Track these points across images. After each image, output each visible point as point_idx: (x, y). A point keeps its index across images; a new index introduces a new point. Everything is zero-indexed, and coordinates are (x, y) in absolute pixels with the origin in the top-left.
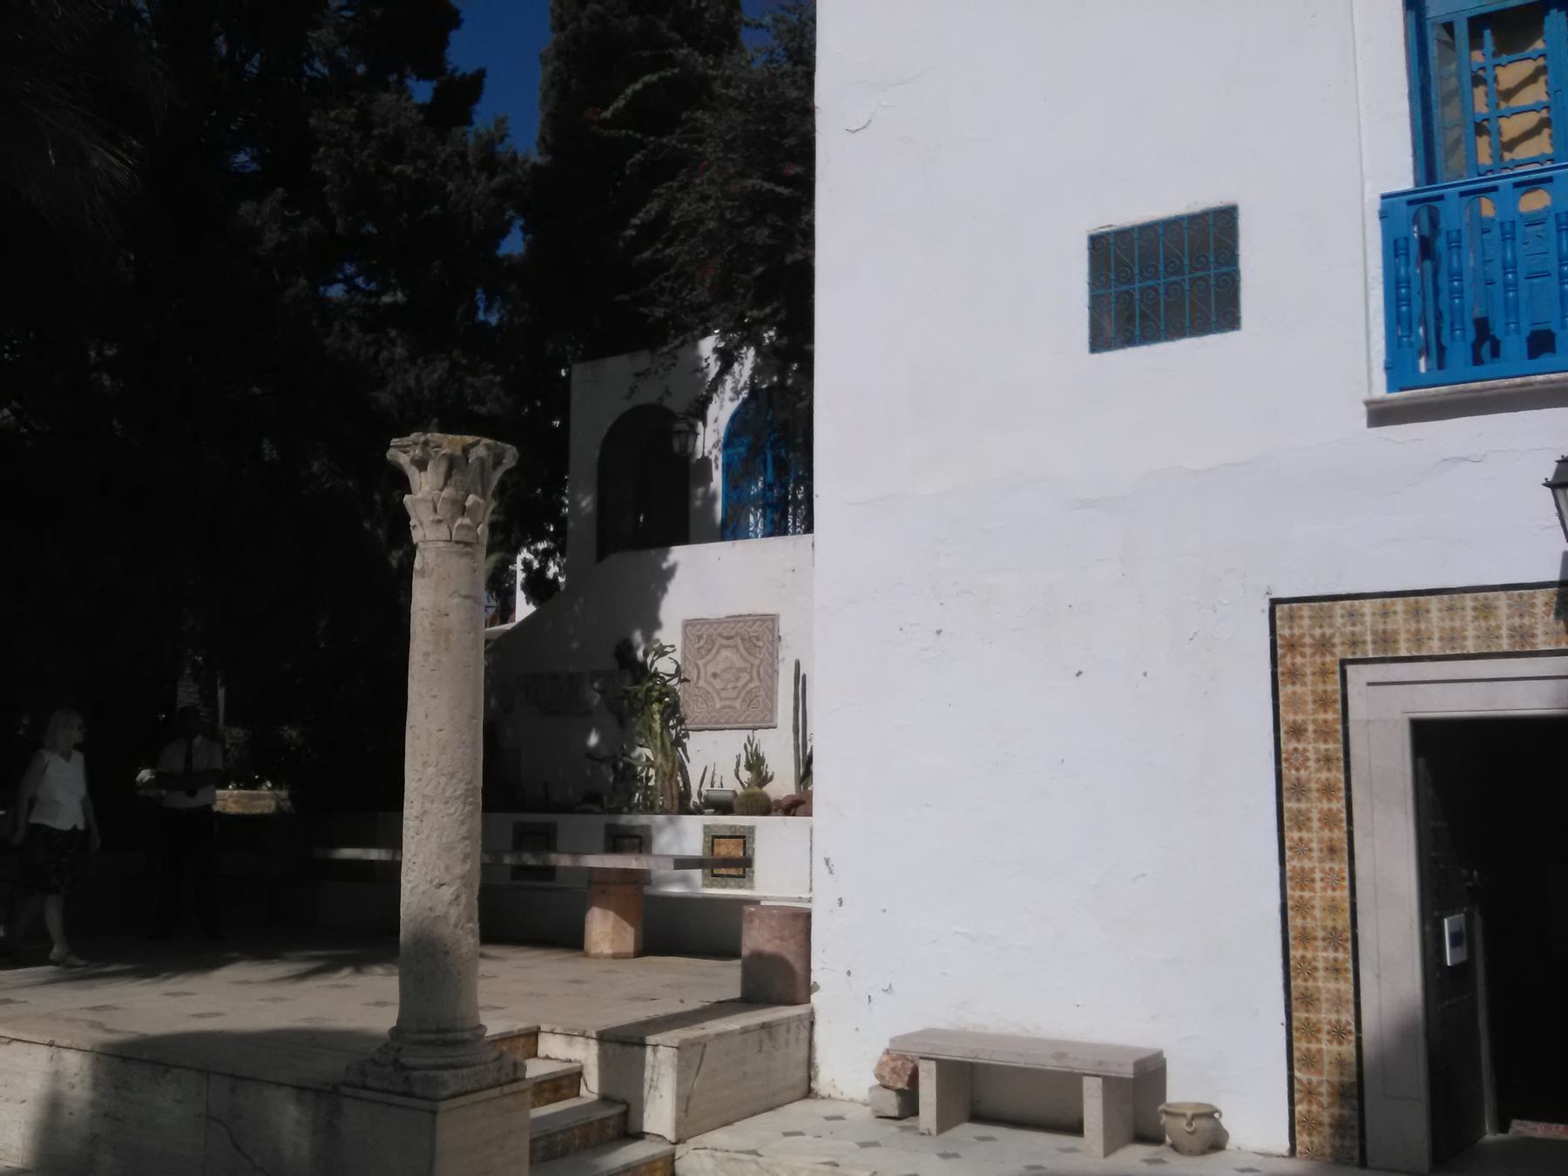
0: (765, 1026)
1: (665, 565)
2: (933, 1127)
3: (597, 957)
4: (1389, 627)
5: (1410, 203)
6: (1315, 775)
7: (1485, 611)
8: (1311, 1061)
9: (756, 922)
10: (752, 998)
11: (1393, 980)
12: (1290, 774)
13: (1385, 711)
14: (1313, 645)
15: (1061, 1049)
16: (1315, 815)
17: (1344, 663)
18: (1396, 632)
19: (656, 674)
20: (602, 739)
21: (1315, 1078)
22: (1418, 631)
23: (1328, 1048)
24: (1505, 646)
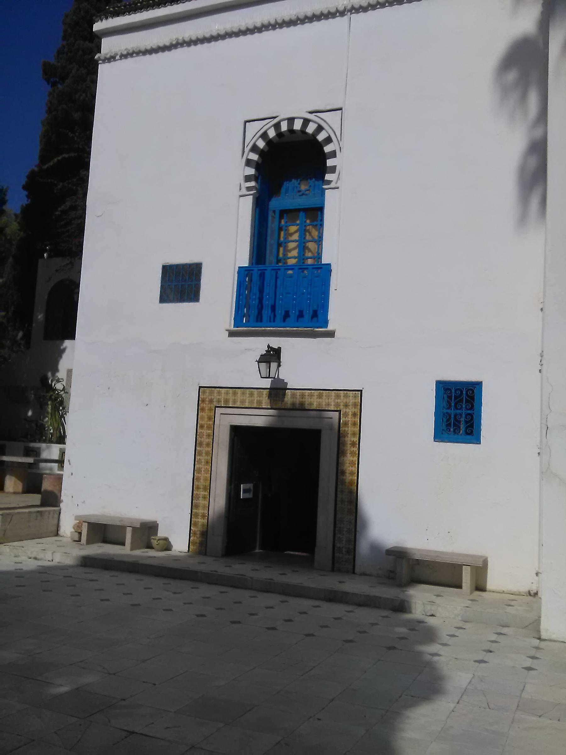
0: (38, 512)
1: (62, 347)
2: (85, 543)
3: (7, 493)
4: (228, 397)
5: (246, 270)
6: (205, 440)
7: (251, 395)
8: (196, 524)
9: (46, 480)
10: (43, 505)
11: (218, 501)
12: (199, 439)
13: (225, 421)
14: (209, 399)
15: (122, 520)
16: (204, 452)
17: (216, 407)
18: (229, 399)
19: (56, 390)
20: (33, 413)
21: (196, 529)
22: (235, 399)
23: (201, 521)
24: (255, 406)
